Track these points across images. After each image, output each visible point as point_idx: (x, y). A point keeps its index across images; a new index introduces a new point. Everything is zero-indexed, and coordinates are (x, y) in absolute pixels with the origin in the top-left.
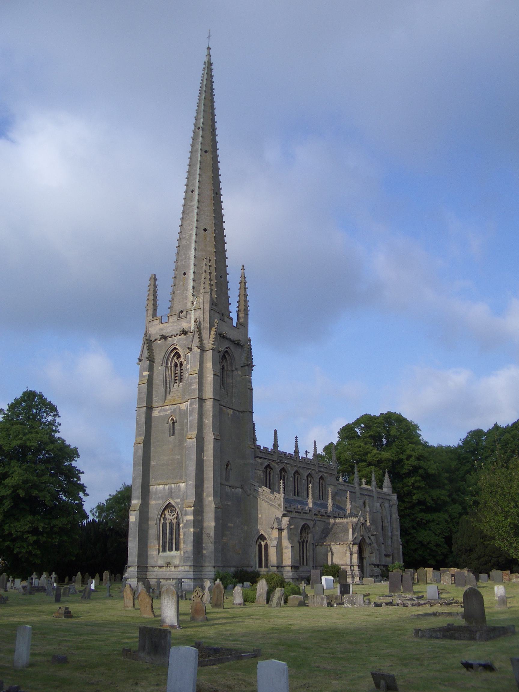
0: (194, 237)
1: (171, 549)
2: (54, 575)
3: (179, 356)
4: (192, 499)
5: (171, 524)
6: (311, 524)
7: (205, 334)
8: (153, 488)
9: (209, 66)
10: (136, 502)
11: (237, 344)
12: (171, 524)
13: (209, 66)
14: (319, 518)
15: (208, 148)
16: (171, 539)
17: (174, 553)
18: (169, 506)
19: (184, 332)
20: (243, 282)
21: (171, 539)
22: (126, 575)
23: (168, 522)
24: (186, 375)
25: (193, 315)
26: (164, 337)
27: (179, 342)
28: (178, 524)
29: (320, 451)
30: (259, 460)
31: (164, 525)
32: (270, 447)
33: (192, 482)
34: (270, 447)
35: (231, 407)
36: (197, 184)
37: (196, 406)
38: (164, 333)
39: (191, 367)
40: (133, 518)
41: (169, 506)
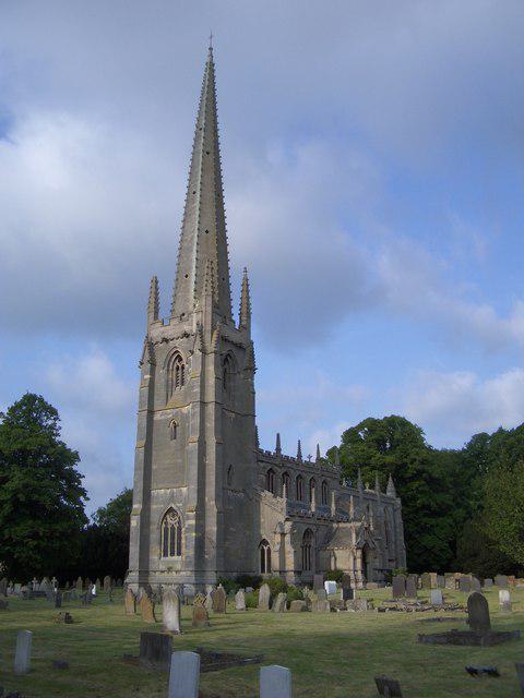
5: (173, 528)
6: (314, 528)
9: (211, 66)
11: (240, 347)
12: (173, 528)
13: (211, 66)
14: (322, 522)
20: (246, 284)
23: (169, 527)
28: (180, 529)
30: (262, 465)
31: (166, 529)
32: (273, 451)
34: (273, 451)
38: (166, 335)
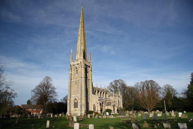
0: (80, 45)
1: (76, 108)
2: (63, 113)
3: (77, 69)
4: (80, 97)
7: (82, 65)
8: (72, 96)
10: (69, 98)
15: (83, 26)
16: (76, 106)
17: (77, 108)
18: (75, 99)
19: (78, 64)
21: (76, 106)
22: (67, 113)
24: (78, 72)
25: (80, 61)
26: (74, 65)
27: (77, 66)
28: (77, 103)
29: (106, 87)
31: (75, 103)
33: (80, 94)
35: (86, 38)
36: (80, 34)
37: (80, 79)
39: (79, 70)
40: (68, 101)
41: (75, 99)
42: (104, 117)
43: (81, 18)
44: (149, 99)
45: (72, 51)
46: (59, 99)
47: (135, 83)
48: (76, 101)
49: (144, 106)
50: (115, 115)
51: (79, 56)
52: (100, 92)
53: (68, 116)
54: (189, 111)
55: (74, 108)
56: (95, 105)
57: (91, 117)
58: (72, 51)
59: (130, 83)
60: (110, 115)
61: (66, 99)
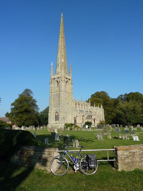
17: (57, 121)
28: (58, 116)
31: (55, 116)
42: (84, 130)
43: (61, 27)
44: (60, 163)
45: (52, 64)
46: (41, 108)
47: (119, 95)
48: (57, 114)
49: (124, 120)
50: (92, 128)
51: (60, 69)
52: (81, 104)
53: (50, 129)
54: (25, 178)
55: (55, 121)
56: (75, 118)
57: (71, 129)
58: (52, 64)
59: (113, 95)
60: (89, 128)
61: (47, 111)
